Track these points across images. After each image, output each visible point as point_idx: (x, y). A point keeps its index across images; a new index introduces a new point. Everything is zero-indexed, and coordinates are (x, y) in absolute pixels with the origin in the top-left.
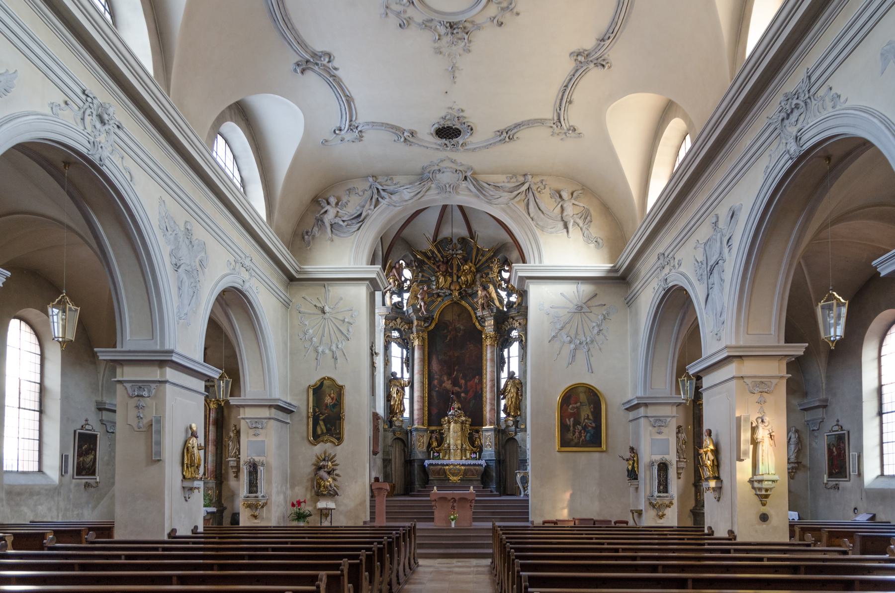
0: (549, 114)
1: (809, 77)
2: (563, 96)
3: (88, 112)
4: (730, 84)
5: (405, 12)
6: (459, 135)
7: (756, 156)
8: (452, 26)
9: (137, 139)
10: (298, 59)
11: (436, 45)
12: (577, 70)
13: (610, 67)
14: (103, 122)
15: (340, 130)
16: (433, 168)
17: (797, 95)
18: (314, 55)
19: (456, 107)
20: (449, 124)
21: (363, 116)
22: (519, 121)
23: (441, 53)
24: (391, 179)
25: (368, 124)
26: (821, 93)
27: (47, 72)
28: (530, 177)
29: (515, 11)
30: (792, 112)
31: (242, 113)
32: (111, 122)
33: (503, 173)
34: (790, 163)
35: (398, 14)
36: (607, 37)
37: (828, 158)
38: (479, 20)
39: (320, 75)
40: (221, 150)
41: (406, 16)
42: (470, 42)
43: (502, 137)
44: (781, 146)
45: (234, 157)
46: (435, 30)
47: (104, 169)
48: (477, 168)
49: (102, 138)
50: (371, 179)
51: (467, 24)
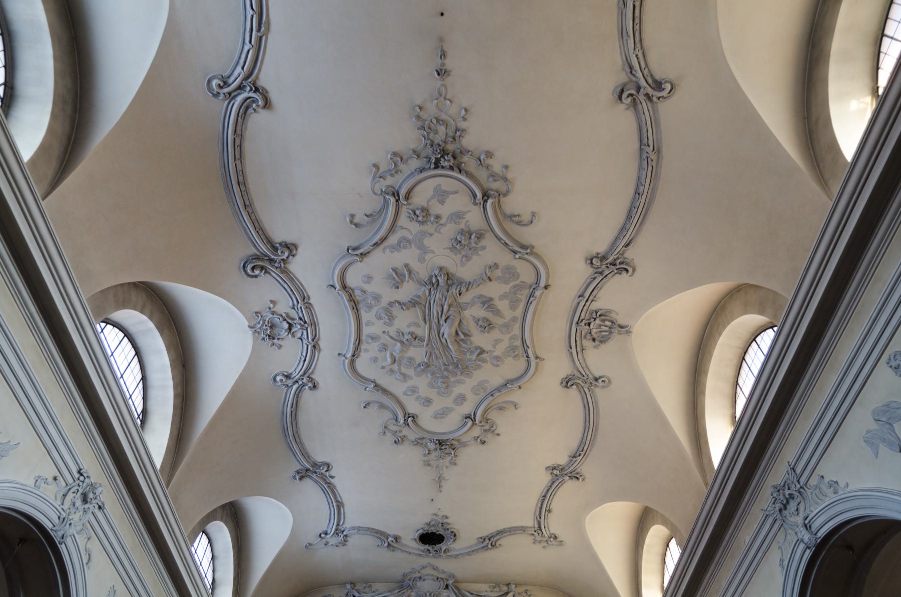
0: (529, 521)
1: (793, 469)
2: (542, 505)
3: (74, 489)
4: (706, 491)
5: (400, 431)
6: (443, 541)
7: (763, 550)
8: (440, 443)
9: (115, 522)
10: (299, 467)
11: (426, 458)
12: (553, 482)
13: (583, 480)
14: (85, 500)
15: (326, 534)
16: (414, 576)
17: (786, 485)
18: (315, 465)
19: (441, 514)
20: (433, 529)
21: (351, 520)
22: (501, 528)
23: (429, 465)
24: (370, 586)
25: (354, 528)
26: (813, 481)
27: (50, 450)
28: (513, 586)
29: (496, 432)
30: (788, 502)
31: (235, 517)
32: (94, 501)
33: (485, 582)
34: (808, 554)
35: (394, 433)
36: (580, 453)
37: (850, 548)
38: (464, 439)
39: (316, 482)
40: (201, 547)
41: (401, 435)
42: (456, 456)
43: (485, 544)
44: (789, 537)
45: (213, 558)
46: (426, 446)
47: (62, 548)
48: (459, 576)
49: (75, 517)
50: (348, 586)
51: (454, 442)
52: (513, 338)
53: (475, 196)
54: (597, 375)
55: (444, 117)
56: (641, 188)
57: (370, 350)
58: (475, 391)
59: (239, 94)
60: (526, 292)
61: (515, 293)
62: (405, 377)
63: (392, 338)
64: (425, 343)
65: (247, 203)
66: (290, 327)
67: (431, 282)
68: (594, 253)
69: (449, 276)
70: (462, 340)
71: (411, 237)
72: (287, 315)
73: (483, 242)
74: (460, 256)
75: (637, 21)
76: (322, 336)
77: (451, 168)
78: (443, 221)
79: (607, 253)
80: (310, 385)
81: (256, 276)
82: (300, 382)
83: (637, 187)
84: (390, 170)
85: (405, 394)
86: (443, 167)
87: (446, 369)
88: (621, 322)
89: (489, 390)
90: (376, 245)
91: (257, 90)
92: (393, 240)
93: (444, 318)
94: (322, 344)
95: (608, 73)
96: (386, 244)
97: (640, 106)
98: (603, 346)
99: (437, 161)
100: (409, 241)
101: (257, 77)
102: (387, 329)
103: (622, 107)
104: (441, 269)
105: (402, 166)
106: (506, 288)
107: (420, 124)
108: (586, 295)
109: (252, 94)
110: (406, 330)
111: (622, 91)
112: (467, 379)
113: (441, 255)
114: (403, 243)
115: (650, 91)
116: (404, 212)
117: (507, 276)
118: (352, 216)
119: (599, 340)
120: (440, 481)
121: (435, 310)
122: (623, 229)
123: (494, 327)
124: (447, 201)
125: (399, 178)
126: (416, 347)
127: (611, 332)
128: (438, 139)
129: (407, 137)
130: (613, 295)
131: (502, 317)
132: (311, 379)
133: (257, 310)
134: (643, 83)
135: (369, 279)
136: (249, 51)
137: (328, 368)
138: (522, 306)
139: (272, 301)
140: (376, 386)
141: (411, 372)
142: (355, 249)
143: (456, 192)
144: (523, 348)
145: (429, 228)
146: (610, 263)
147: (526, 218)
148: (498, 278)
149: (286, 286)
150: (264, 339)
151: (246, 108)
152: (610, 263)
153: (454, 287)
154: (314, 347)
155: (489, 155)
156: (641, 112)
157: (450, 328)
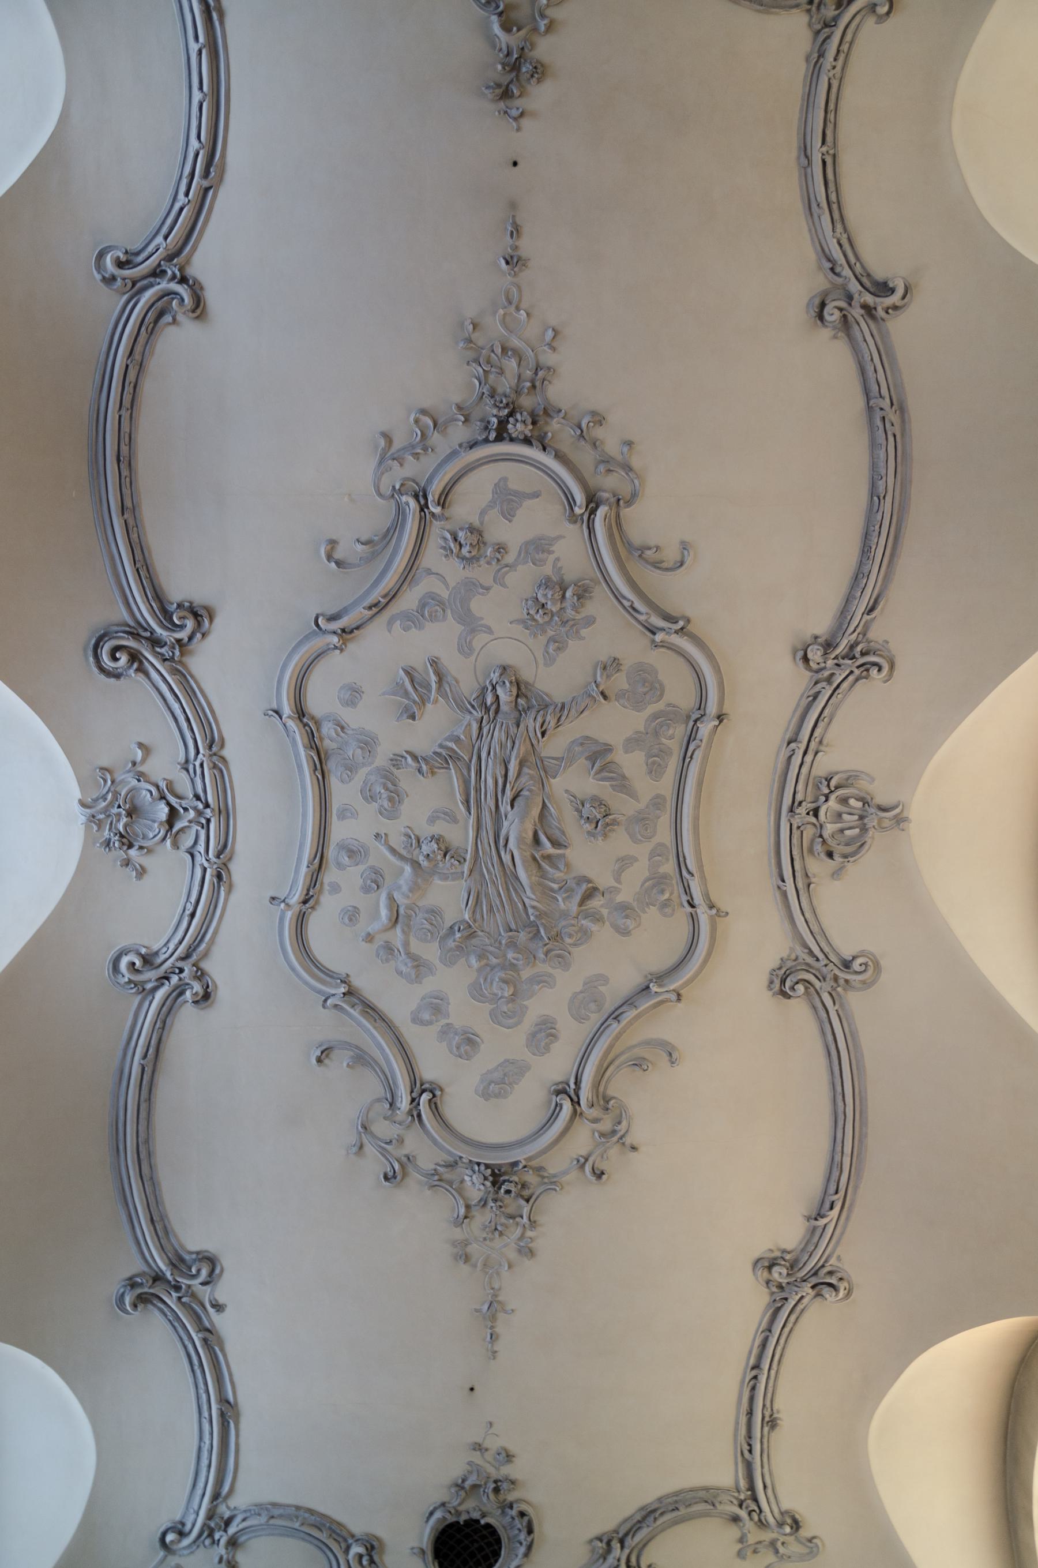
0: (722, 1472)
8: (496, 1177)
10: (137, 1266)
15: (182, 1534)
18: (178, 1262)
23: (467, 1258)
25: (260, 1508)
29: (628, 1140)
36: (833, 1198)
51: (531, 1178)
52: (657, 852)
53: (571, 502)
54: (847, 955)
55: (515, 342)
56: (881, 484)
57: (344, 882)
58: (577, 1008)
59: (151, 285)
60: (680, 731)
61: (656, 734)
62: (419, 967)
63: (393, 851)
64: (466, 868)
65: (128, 503)
66: (173, 814)
67: (483, 703)
68: (808, 637)
69: (520, 688)
70: (548, 858)
71: (445, 594)
72: (170, 786)
73: (590, 608)
74: (543, 639)
75: (832, 186)
76: (239, 847)
77: (527, 441)
78: (510, 558)
79: (834, 635)
80: (197, 987)
81: (118, 676)
82: (175, 979)
83: (873, 486)
84: (413, 447)
85: (416, 1020)
86: (512, 440)
87: (512, 944)
88: (881, 799)
89: (609, 1007)
90: (378, 608)
91: (183, 280)
92: (409, 600)
93: (509, 794)
94: (238, 870)
95: (792, 275)
96: (394, 609)
97: (856, 327)
98: (854, 869)
99: (503, 423)
100: (441, 603)
101: (188, 261)
102: (385, 826)
103: (826, 333)
104: (504, 669)
105: (435, 438)
106: (637, 720)
107: (471, 355)
108: (803, 737)
109: (174, 286)
110: (426, 830)
111: (823, 305)
112: (557, 973)
113: (508, 644)
114: (430, 609)
115: (869, 299)
116: (437, 532)
117: (641, 690)
118: (333, 543)
119: (840, 851)
120: (493, 1318)
121: (491, 772)
122: (858, 577)
123: (615, 822)
124: (518, 512)
125: (429, 462)
126: (445, 878)
127: (864, 829)
128: (505, 385)
129: (448, 381)
130: (857, 738)
131: (632, 794)
132: (200, 975)
133: (105, 764)
134: (854, 286)
135: (353, 695)
136: (181, 209)
137: (243, 951)
138: (673, 764)
139: (141, 745)
140: (350, 993)
141: (430, 951)
142: (332, 618)
143: (536, 495)
144: (679, 882)
145: (483, 573)
146: (843, 657)
147: (671, 554)
148: (621, 695)
149: (176, 706)
150: (108, 843)
151: (159, 314)
152: (843, 657)
153: (532, 714)
154: (219, 876)
155: (599, 419)
156: (860, 339)
157: (522, 821)
